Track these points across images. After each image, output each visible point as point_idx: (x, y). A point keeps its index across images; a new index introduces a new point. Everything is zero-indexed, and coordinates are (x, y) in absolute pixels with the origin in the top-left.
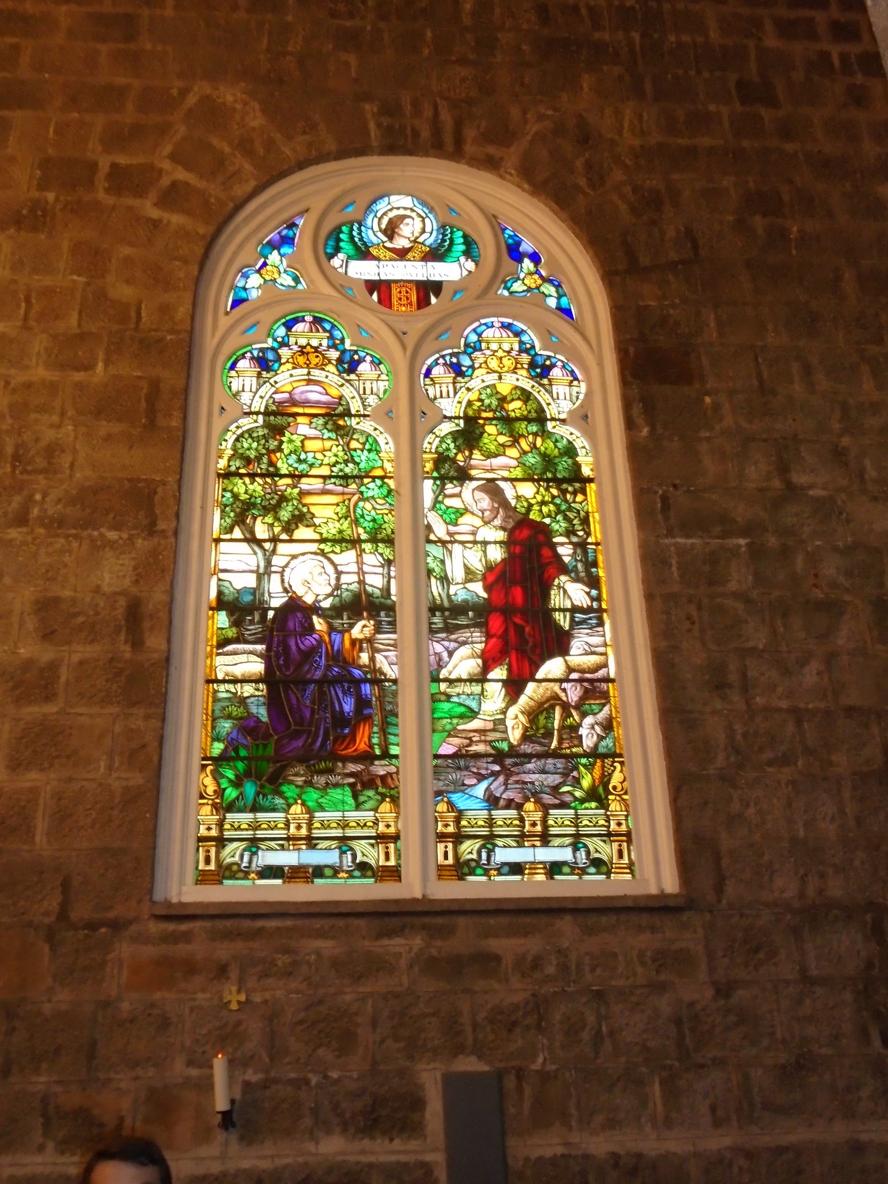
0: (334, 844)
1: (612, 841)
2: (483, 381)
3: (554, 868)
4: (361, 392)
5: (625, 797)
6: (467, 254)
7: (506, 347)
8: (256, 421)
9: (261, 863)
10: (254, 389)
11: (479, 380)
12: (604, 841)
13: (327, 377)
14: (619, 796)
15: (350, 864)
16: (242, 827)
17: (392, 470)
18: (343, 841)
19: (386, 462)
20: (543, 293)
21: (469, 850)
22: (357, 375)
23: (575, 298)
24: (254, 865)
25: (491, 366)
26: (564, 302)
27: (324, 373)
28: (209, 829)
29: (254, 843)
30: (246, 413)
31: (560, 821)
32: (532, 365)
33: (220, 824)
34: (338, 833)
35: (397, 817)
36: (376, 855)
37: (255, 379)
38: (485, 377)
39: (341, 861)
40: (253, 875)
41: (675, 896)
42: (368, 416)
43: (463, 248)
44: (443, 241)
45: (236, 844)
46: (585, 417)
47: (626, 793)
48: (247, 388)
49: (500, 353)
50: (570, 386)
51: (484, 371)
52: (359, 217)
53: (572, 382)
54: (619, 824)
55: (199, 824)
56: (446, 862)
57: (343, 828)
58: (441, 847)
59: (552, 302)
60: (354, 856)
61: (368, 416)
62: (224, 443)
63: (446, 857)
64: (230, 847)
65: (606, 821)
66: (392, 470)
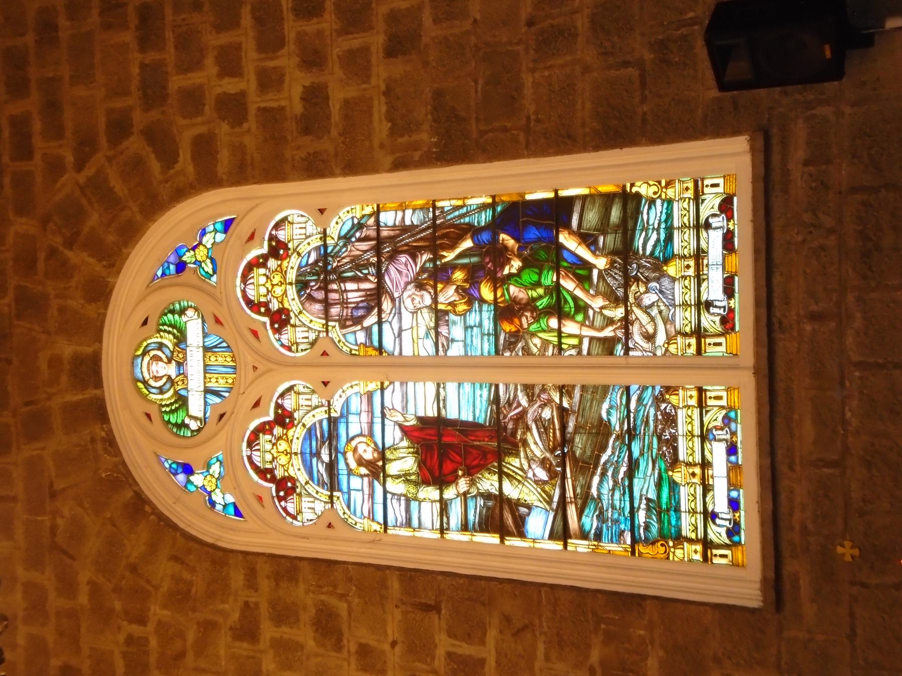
0: (707, 446)
1: (703, 194)
2: (293, 299)
3: (732, 450)
4: (309, 408)
5: (663, 184)
6: (182, 312)
7: (263, 280)
8: (338, 498)
9: (726, 510)
10: (312, 499)
11: (298, 473)
12: (703, 201)
13: (292, 268)
14: (662, 188)
15: (724, 432)
16: (694, 522)
17: (370, 207)
18: (704, 438)
19: (364, 213)
20: (212, 244)
21: (712, 324)
22: (289, 242)
23: (213, 218)
24: (728, 517)
25: (281, 293)
26: (219, 227)
27: (295, 440)
28: (687, 189)
29: (710, 516)
30: (332, 506)
31: (690, 452)
32: (277, 256)
33: (688, 464)
34: (697, 441)
35: (683, 388)
36: (715, 409)
37: (297, 329)
38: (296, 468)
39: (720, 440)
40: (731, 223)
41: (752, 141)
42: (329, 402)
43: (176, 316)
44: (174, 335)
45: (709, 531)
46: (322, 211)
47: (660, 183)
48: (311, 505)
49: (269, 285)
50: (293, 223)
51: (291, 468)
52: (156, 406)
53: (289, 222)
54: (691, 397)
55: (690, 561)
56: (722, 185)
57: (693, 436)
58: (716, 561)
59: (220, 237)
60: (714, 215)
61: (329, 402)
62: (358, 526)
63: (716, 185)
64: (712, 536)
65: (686, 279)
66: (370, 207)
